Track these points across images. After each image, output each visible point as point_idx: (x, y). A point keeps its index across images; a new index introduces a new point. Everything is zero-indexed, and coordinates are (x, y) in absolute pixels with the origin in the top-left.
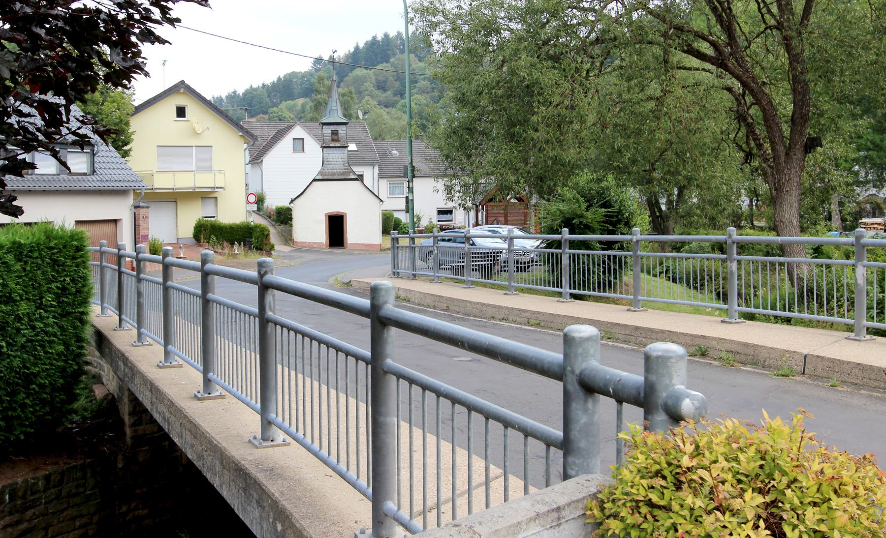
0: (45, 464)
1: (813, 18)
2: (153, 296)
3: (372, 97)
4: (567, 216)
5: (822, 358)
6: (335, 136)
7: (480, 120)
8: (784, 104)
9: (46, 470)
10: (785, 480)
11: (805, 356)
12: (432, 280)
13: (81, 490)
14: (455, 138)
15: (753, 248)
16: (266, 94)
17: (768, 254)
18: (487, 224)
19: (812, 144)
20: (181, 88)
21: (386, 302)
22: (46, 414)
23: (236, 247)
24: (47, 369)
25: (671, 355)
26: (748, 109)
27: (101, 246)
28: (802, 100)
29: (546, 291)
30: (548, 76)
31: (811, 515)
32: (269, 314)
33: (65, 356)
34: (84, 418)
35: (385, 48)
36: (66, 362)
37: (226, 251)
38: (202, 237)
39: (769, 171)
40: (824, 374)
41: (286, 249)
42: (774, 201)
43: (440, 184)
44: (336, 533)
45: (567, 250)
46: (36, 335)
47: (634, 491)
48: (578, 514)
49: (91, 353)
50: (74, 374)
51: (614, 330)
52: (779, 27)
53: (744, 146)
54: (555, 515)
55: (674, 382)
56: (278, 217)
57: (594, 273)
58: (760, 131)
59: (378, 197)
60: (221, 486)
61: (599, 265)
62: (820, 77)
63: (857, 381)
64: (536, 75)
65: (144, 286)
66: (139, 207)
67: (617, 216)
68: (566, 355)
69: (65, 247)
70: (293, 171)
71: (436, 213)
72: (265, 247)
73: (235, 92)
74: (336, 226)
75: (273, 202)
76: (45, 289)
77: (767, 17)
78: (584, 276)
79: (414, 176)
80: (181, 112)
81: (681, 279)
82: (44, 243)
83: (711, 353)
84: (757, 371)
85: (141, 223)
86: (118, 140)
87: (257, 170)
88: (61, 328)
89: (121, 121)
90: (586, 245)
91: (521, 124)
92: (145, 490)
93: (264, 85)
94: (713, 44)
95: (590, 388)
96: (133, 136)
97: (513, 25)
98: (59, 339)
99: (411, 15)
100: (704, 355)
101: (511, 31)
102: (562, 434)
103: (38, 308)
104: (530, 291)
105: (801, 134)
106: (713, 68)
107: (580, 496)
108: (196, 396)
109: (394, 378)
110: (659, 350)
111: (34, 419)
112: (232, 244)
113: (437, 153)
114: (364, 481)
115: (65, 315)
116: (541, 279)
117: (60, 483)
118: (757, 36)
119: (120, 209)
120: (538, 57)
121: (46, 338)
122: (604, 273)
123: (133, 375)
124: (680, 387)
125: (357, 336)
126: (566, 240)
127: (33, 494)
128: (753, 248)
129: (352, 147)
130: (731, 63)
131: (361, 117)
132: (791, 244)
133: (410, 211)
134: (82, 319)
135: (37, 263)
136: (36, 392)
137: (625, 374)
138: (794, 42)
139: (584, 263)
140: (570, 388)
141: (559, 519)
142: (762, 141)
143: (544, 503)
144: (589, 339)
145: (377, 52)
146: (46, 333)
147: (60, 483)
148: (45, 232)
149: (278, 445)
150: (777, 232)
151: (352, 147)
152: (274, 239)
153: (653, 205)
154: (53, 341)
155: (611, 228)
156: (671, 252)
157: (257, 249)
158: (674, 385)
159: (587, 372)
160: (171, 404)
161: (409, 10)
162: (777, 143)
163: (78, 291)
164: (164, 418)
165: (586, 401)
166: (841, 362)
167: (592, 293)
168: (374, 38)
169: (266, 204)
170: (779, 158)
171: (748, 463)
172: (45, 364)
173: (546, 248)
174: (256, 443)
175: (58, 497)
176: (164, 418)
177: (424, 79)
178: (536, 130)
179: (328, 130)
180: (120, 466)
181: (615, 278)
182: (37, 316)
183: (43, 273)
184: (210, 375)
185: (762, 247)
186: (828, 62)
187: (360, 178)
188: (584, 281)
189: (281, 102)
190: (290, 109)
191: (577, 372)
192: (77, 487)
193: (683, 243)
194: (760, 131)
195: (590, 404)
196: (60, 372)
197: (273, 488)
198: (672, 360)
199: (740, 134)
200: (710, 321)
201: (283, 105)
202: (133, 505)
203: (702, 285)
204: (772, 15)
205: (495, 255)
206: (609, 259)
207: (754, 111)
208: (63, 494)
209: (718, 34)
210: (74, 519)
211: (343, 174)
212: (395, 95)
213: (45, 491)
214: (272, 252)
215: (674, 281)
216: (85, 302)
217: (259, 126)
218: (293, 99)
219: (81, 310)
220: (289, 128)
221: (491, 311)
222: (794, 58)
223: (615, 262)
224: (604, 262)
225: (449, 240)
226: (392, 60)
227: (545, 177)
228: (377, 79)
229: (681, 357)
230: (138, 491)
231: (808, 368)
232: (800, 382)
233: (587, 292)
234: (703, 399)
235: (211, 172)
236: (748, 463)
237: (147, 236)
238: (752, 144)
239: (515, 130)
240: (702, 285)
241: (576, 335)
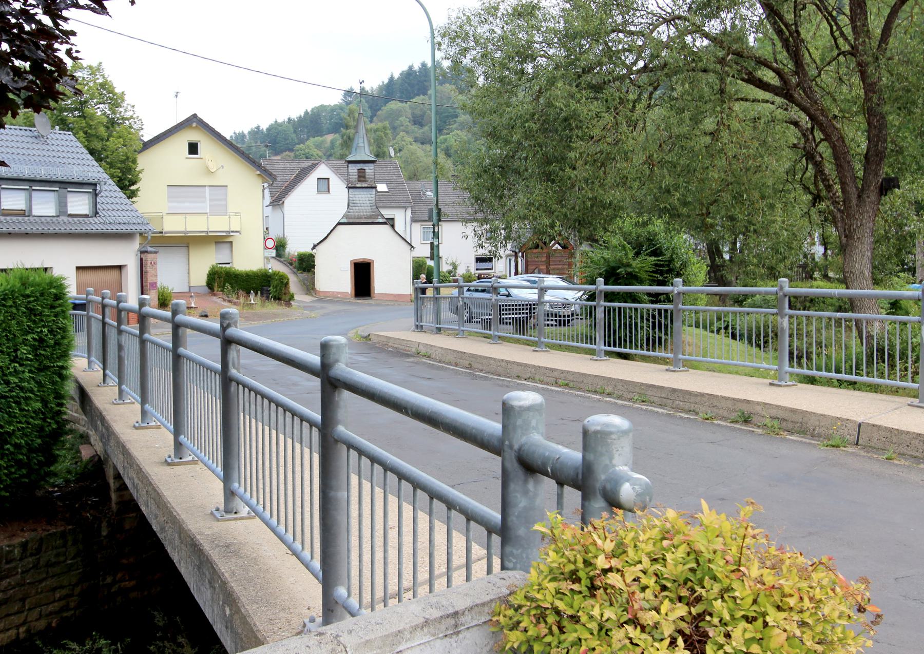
0: (22, 530)
1: (892, 42)
2: (132, 348)
3: (407, 132)
4: (612, 264)
5: (879, 427)
6: (362, 175)
7: (513, 157)
8: (857, 139)
9: (23, 537)
10: (717, 588)
11: (860, 425)
12: (458, 334)
13: (62, 559)
14: (485, 177)
15: (824, 302)
16: (292, 130)
17: (839, 309)
18: (527, 273)
19: (888, 186)
20: (194, 122)
21: (337, 361)
22: (22, 476)
23: (252, 296)
24: (23, 428)
25: (613, 430)
26: (817, 146)
27: (88, 294)
28: (877, 136)
29: (590, 349)
30: (587, 108)
31: (740, 632)
32: (233, 372)
33: (43, 413)
34: (67, 481)
36: (44, 420)
37: (242, 300)
38: (216, 285)
39: (839, 215)
40: (880, 445)
41: (307, 299)
42: (844, 249)
43: (469, 229)
44: (283, 620)
45: (602, 303)
46: (11, 391)
47: (539, 596)
48: (483, 620)
49: (72, 410)
50: (54, 433)
51: (649, 393)
52: (854, 52)
53: (812, 187)
54: (452, 621)
55: (614, 462)
57: (642, 328)
58: (829, 168)
59: (410, 244)
60: (180, 562)
61: (648, 320)
62: (899, 108)
63: (917, 454)
64: (573, 105)
65: (124, 339)
66: (146, 252)
67: (668, 266)
68: (504, 427)
69: (42, 294)
70: (316, 213)
72: (284, 297)
73: (258, 128)
74: (362, 274)
75: (295, 248)
76: (20, 340)
77: (841, 41)
78: (631, 332)
79: (439, 220)
80: (193, 148)
81: (741, 336)
82: (19, 290)
83: (755, 419)
84: (804, 440)
85: (149, 269)
86: (125, 179)
87: (278, 213)
88: (39, 383)
89: (128, 158)
90: (632, 297)
91: (557, 161)
92: (131, 560)
93: (289, 119)
94: (778, 72)
95: (530, 467)
96: (140, 175)
97: (551, 52)
98: (37, 395)
99: (438, 39)
100: (746, 421)
101: (549, 57)
102: (500, 517)
103: (12, 361)
104: (560, 348)
105: (876, 174)
106: (779, 100)
107: (488, 598)
108: (166, 461)
109: (345, 448)
110: (598, 424)
111: (9, 482)
112: (248, 293)
113: (467, 195)
114: (317, 564)
115: (42, 369)
116: (582, 334)
117: (38, 551)
118: (829, 64)
119: (125, 255)
120: (577, 86)
121: (22, 394)
122: (654, 328)
123: (109, 436)
124: (622, 468)
125: (305, 395)
126: (601, 292)
127: (8, 562)
128: (824, 302)
129: (382, 187)
130: (798, 94)
131: (392, 154)
132: (861, 298)
133: (435, 258)
134: (61, 374)
135: (11, 312)
136: (12, 453)
137: (566, 450)
138: (871, 69)
139: (631, 317)
140: (508, 465)
141: (456, 626)
142: (831, 182)
143: (438, 606)
144: (529, 408)
145: (411, 84)
146: (22, 389)
147: (38, 551)
148: (21, 279)
149: (242, 518)
150: (846, 284)
151: (382, 187)
153: (714, 251)
154: (30, 398)
155: (661, 278)
156: (733, 305)
157: (275, 299)
158: (614, 466)
159: (526, 448)
160: (140, 470)
161: (436, 34)
162: (849, 186)
163: (57, 343)
164: (133, 484)
165: (526, 482)
166: (900, 432)
167: (639, 352)
168: (411, 68)
169: (287, 250)
170: (850, 201)
171: (676, 565)
172: (20, 422)
173: (588, 300)
174: (218, 515)
175: (36, 566)
176: (133, 484)
178: (574, 169)
179: (354, 169)
180: (104, 533)
181: (666, 334)
182: (12, 370)
183: (18, 323)
184: (182, 438)
185: (834, 301)
186: (909, 91)
187: (390, 222)
188: (631, 337)
189: (307, 139)
190: (318, 146)
191: (516, 447)
192: (57, 555)
193: (746, 296)
194: (829, 168)
195: (531, 486)
196: (37, 431)
197: (224, 567)
198: (613, 437)
199: (808, 174)
200: (757, 384)
201: (311, 142)
202: (119, 575)
203: (766, 342)
204: (846, 39)
205: (531, 308)
206: (614, 310)
207: (824, 149)
208: (41, 563)
209: (785, 62)
210: (54, 590)
211: (370, 217)
213: (21, 559)
214: (292, 302)
215: (734, 337)
216: (65, 355)
217: (280, 164)
218: (321, 136)
219: (60, 364)
220: (313, 167)
221: (516, 370)
222: (870, 88)
223: (666, 317)
224: (654, 317)
225: (483, 291)
228: (413, 114)
229: (625, 433)
230: (125, 561)
231: (862, 437)
232: (852, 454)
233: (633, 351)
234: (647, 484)
235: (226, 214)
236: (675, 564)
237: (156, 283)
238: (821, 186)
239: (551, 169)
240: (766, 342)
241: (516, 403)
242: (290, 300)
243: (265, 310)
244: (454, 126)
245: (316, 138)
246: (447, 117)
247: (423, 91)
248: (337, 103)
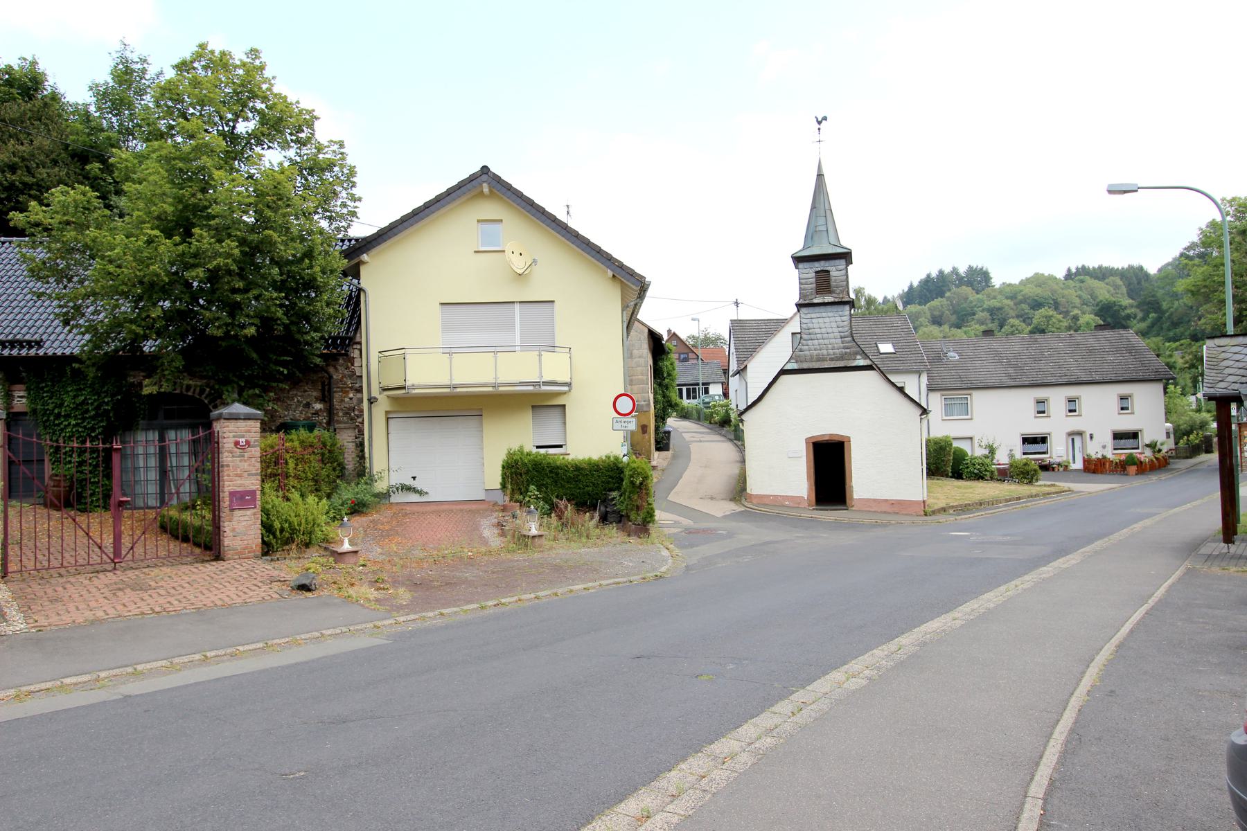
71: (1019, 441)
74: (829, 464)
168: (928, 276)
177: (983, 311)
211: (841, 358)
226: (948, 294)
227: (628, 516)
243: (50, 618)
247: (941, 294)
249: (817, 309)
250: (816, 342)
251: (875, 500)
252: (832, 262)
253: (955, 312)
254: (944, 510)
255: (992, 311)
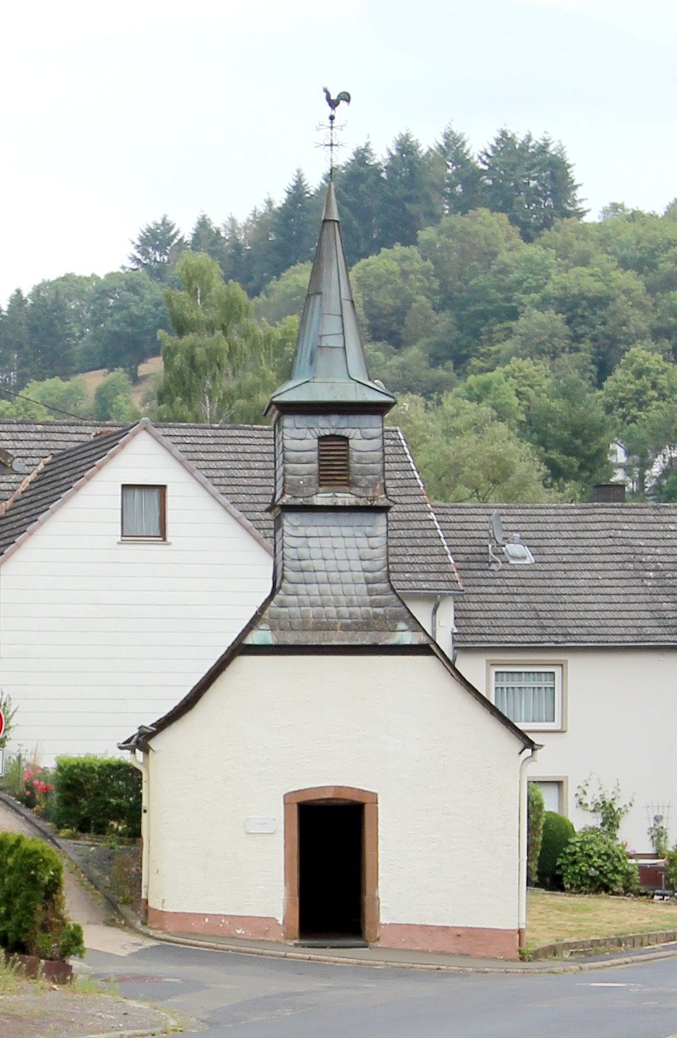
6: (334, 462)
35: (401, 191)
56: (67, 802)
72: (41, 940)
74: (331, 847)
152: (75, 906)
177: (543, 304)
179: (301, 438)
189: (21, 386)
201: (34, 390)
211: (366, 625)
212: (435, 360)
218: (65, 376)
220: (104, 445)
226: (426, 234)
228: (369, 304)
242: (66, 952)
244: (508, 345)
245: (50, 383)
246: (484, 315)
247: (401, 230)
248: (116, 269)
249: (318, 518)
250: (314, 588)
251: (423, 927)
252: (355, 420)
253: (447, 302)
254: (553, 951)
255: (575, 309)
